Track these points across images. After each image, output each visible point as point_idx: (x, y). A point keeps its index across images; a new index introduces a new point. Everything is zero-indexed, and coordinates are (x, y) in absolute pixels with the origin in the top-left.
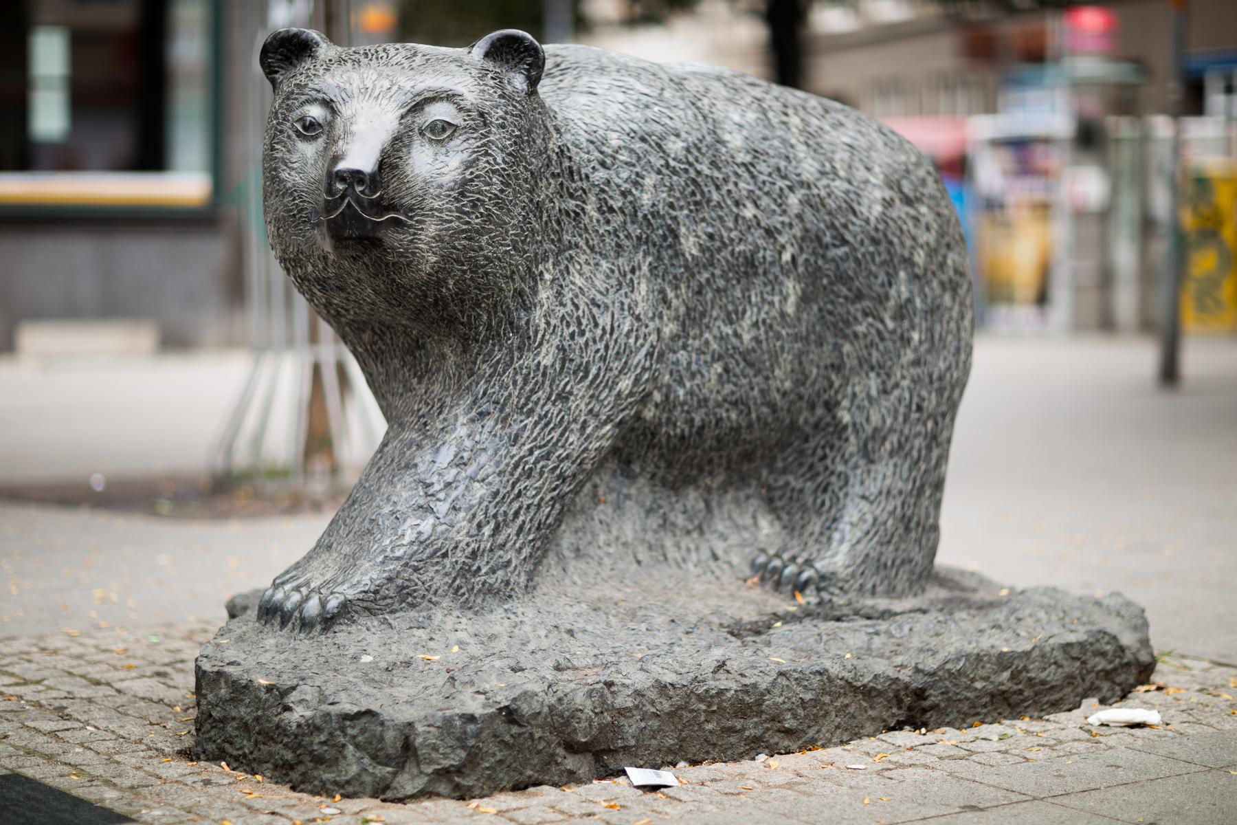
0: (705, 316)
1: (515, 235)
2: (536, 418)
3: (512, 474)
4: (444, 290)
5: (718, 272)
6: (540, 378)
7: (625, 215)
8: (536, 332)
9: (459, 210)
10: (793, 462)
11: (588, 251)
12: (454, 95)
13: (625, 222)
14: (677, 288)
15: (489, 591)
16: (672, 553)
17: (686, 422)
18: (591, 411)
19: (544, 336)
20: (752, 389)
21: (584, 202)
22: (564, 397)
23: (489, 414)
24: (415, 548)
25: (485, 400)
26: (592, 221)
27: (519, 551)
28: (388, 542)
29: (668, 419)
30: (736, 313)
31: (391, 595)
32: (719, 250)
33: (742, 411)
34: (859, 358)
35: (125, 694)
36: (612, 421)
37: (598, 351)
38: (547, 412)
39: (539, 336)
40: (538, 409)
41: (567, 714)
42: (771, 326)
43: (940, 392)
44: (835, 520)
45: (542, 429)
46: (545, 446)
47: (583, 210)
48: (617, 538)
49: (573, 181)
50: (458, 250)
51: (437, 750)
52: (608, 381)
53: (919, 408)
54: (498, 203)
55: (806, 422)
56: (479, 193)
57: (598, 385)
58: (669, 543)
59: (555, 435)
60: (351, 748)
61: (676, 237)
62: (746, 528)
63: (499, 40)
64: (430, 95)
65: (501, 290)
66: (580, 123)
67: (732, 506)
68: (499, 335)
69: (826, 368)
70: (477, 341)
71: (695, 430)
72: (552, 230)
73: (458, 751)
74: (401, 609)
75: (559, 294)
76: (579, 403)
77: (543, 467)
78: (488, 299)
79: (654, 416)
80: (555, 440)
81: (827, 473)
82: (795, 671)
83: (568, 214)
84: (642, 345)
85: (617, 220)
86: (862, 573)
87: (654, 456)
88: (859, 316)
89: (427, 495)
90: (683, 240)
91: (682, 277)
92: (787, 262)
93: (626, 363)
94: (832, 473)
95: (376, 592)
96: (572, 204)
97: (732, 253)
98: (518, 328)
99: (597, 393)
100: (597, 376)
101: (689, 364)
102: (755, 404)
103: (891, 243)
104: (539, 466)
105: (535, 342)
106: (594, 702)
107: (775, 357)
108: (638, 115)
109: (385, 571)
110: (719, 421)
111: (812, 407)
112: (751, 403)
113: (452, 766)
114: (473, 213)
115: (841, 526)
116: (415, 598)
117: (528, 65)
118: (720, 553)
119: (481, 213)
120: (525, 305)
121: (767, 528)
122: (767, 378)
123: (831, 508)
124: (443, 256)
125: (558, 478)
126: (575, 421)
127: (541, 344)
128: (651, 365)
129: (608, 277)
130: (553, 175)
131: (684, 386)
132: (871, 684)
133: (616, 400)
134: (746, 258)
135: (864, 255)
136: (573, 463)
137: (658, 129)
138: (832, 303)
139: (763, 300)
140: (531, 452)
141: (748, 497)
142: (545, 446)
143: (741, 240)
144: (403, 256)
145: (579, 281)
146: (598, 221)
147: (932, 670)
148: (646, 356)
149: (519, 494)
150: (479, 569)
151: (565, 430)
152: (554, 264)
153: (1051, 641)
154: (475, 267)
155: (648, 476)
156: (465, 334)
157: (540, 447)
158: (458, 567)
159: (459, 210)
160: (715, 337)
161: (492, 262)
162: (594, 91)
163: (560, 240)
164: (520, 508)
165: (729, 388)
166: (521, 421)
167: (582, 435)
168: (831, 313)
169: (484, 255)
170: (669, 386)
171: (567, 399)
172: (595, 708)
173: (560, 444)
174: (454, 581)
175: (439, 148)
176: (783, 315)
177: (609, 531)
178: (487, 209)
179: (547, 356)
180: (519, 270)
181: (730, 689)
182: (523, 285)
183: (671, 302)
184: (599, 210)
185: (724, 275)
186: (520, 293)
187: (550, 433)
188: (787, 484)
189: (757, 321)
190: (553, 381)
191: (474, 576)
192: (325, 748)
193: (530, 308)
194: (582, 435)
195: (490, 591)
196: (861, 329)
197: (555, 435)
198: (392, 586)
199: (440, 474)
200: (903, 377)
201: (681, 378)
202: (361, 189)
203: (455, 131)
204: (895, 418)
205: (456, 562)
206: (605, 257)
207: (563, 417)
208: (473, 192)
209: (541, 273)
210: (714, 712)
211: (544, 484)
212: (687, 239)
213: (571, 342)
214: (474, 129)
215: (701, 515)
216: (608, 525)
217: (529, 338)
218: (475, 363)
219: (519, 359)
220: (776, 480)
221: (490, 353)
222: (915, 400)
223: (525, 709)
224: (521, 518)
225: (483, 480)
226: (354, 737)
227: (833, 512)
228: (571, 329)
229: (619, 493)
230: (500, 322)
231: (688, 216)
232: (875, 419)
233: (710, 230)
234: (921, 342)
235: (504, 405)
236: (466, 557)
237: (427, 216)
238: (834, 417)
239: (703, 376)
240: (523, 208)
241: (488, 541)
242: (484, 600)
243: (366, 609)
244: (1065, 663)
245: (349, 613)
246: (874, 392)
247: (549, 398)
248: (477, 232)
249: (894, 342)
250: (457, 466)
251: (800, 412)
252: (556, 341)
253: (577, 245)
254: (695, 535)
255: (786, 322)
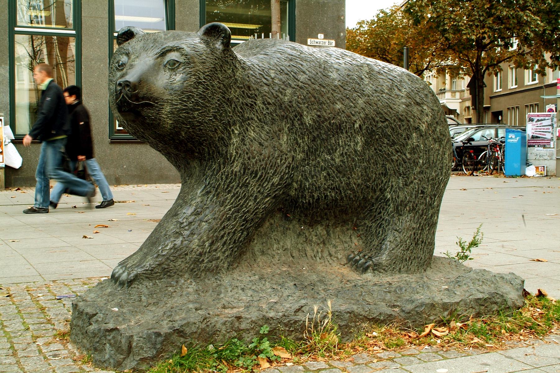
0: (317, 151)
1: (214, 112)
2: (232, 194)
3: (221, 219)
4: (181, 137)
5: (323, 132)
6: (233, 176)
7: (276, 106)
8: (231, 157)
9: (180, 100)
10: (367, 215)
11: (258, 121)
12: (180, 48)
13: (276, 109)
14: (303, 138)
15: (208, 270)
16: (310, 253)
17: (310, 197)
18: (259, 191)
19: (235, 158)
20: (342, 183)
21: (256, 100)
22: (246, 185)
23: (211, 192)
24: (172, 251)
25: (209, 186)
26: (260, 108)
27: (224, 252)
28: (160, 248)
29: (302, 196)
30: (332, 150)
31: (159, 271)
32: (323, 122)
33: (337, 192)
34: (394, 170)
35: (470, 252)
36: (270, 196)
37: (262, 165)
38: (237, 192)
39: (233, 158)
40: (233, 191)
41: (211, 333)
42: (349, 155)
43: (433, 185)
44: (384, 239)
45: (235, 199)
46: (237, 206)
47: (255, 103)
48: (283, 247)
49: (250, 90)
50: (182, 118)
51: (143, 349)
52: (267, 178)
53: (423, 192)
54: (202, 97)
55: (372, 197)
56: (190, 92)
57: (262, 180)
58: (308, 249)
59: (242, 202)
60: (108, 345)
61: (301, 116)
62: (346, 242)
63: (210, 27)
64: (169, 48)
65: (211, 137)
66: (256, 66)
67: (340, 233)
68: (213, 157)
69: (379, 174)
70: (205, 160)
71: (315, 200)
72: (238, 112)
73: (153, 350)
74: (164, 278)
75: (243, 140)
76: (253, 187)
77: (236, 216)
78: (206, 142)
79: (295, 194)
80: (242, 204)
81: (381, 219)
82: (337, 311)
83: (247, 105)
84: (284, 163)
85: (272, 108)
86: (395, 263)
87: (298, 212)
88: (394, 151)
89: (180, 228)
90: (305, 118)
91: (305, 134)
92: (357, 128)
93: (276, 170)
94: (383, 220)
95: (152, 270)
96: (249, 101)
97: (330, 123)
98: (222, 154)
99: (262, 184)
100: (261, 176)
101: (311, 171)
102: (343, 189)
103: (409, 121)
104: (234, 216)
105: (230, 161)
106: (227, 327)
107: (352, 170)
108: (287, 63)
109: (157, 261)
110: (326, 196)
111: (375, 191)
112: (341, 189)
113: (149, 357)
114: (188, 101)
115: (386, 243)
116: (171, 273)
117: (222, 37)
118: (333, 253)
119: (192, 101)
120: (225, 144)
121: (356, 242)
122: (349, 178)
123: (382, 234)
124: (175, 121)
125: (244, 220)
126: (252, 196)
127: (233, 162)
128: (289, 171)
129: (268, 133)
130: (238, 87)
131: (309, 181)
132: (377, 317)
133: (271, 186)
134: (337, 126)
135: (395, 126)
136: (251, 214)
137: (295, 70)
138: (381, 146)
139: (345, 144)
140: (230, 210)
141: (348, 229)
142: (237, 206)
143: (334, 118)
144: (154, 120)
145: (252, 134)
146: (263, 108)
147: (408, 311)
148: (286, 167)
149: (224, 228)
150: (203, 260)
151: (247, 200)
152: (239, 127)
153: (471, 297)
154: (193, 126)
155: (297, 220)
156: (200, 157)
157: (235, 207)
158: (193, 259)
159: (180, 100)
160: (322, 160)
161: (202, 124)
162: (268, 54)
163: (242, 116)
164: (225, 234)
165: (330, 182)
166: (226, 196)
167: (255, 202)
168: (380, 151)
169: (196, 121)
170: (301, 181)
171: (247, 186)
172: (227, 329)
173: (244, 206)
174: (190, 266)
175: (172, 72)
176: (355, 151)
177: (279, 244)
178: (195, 100)
179: (237, 167)
180: (219, 128)
181: (301, 320)
182: (223, 135)
183: (300, 145)
184: (263, 103)
185: (326, 133)
186: (222, 139)
187: (239, 201)
188: (365, 224)
189: (343, 153)
190: (240, 178)
191: (201, 264)
192: (98, 344)
193: (228, 146)
194: (255, 202)
195: (208, 270)
196: (395, 158)
197: (242, 202)
198: (160, 268)
199: (187, 219)
200: (415, 179)
201: (307, 178)
202: (128, 89)
203: (180, 64)
204: (411, 197)
205: (192, 258)
206: (266, 124)
207: (245, 194)
208: (188, 92)
209: (233, 130)
210: (292, 331)
211: (236, 223)
212: (307, 117)
213: (248, 161)
214: (188, 63)
215: (324, 237)
216: (278, 241)
217: (228, 159)
218: (205, 170)
219: (224, 168)
220: (361, 223)
221: (211, 166)
222: (421, 188)
223: (188, 330)
224: (225, 238)
225: (207, 221)
226: (110, 340)
227: (383, 236)
228: (248, 156)
229: (284, 227)
230: (213, 152)
231: (307, 107)
232: (401, 196)
233: (319, 113)
234: (423, 164)
235: (217, 189)
236: (197, 255)
237: (165, 102)
238: (384, 196)
239: (317, 177)
240: (218, 100)
241: (208, 248)
242: (205, 274)
243: (147, 277)
244: (477, 308)
245: (139, 279)
246: (401, 185)
247: (238, 186)
248: (191, 110)
249: (411, 164)
250: (195, 215)
251: (369, 193)
252: (241, 161)
253: (252, 119)
254: (321, 245)
255: (357, 154)
